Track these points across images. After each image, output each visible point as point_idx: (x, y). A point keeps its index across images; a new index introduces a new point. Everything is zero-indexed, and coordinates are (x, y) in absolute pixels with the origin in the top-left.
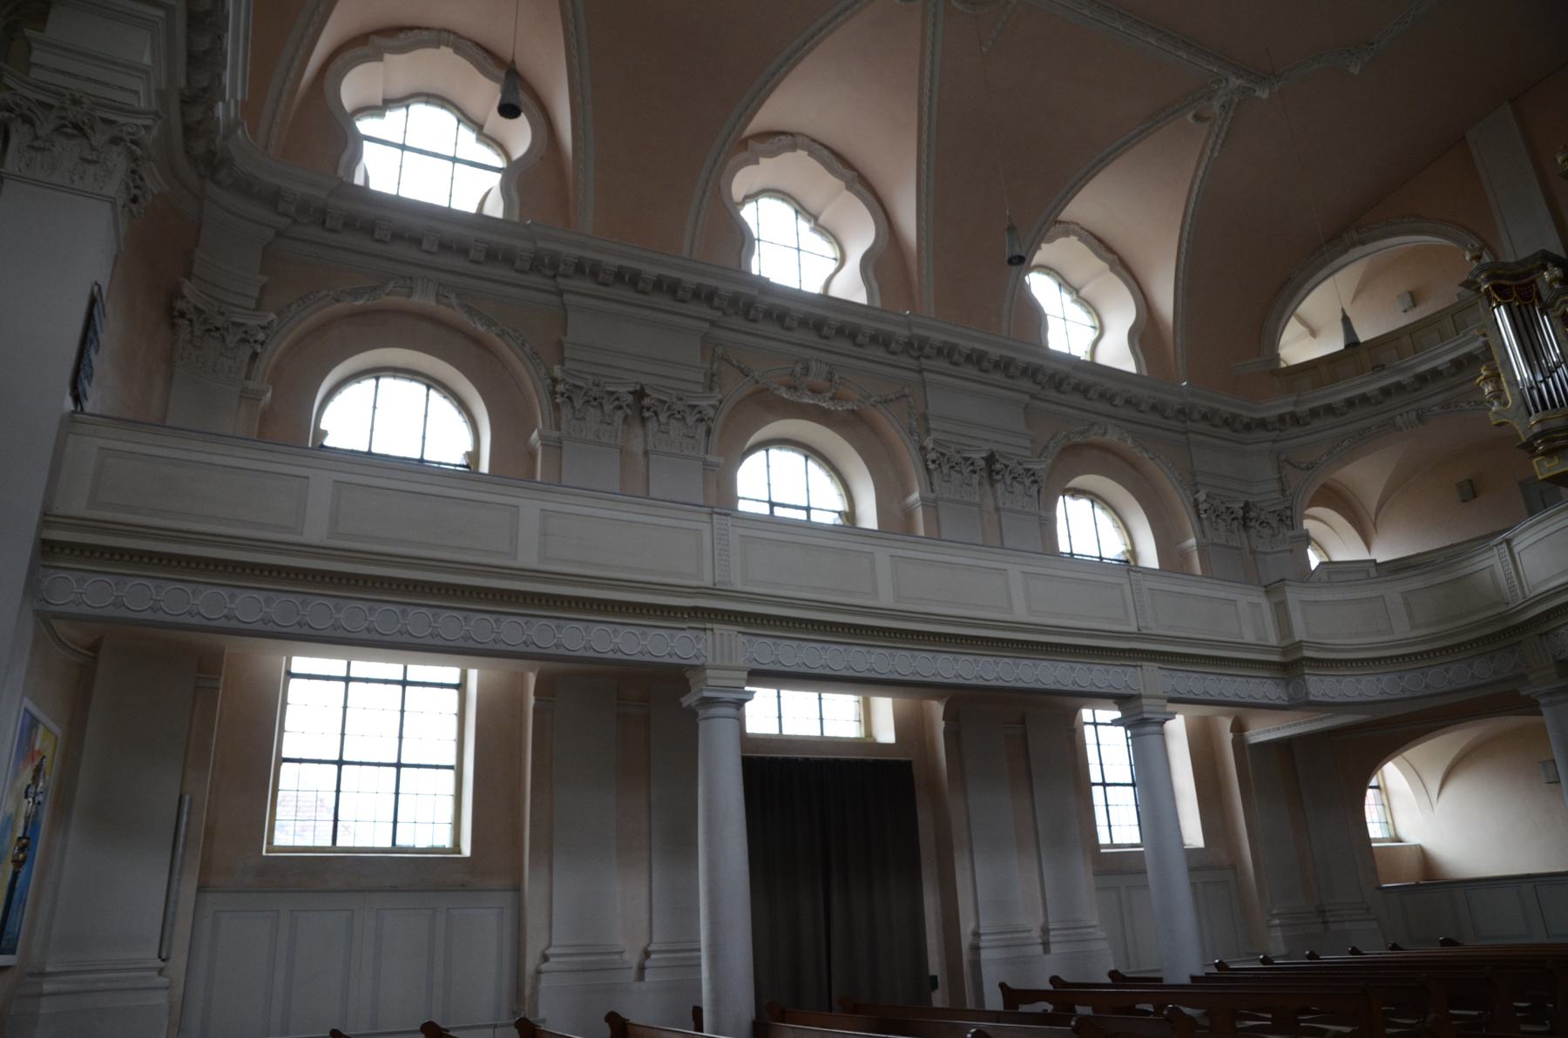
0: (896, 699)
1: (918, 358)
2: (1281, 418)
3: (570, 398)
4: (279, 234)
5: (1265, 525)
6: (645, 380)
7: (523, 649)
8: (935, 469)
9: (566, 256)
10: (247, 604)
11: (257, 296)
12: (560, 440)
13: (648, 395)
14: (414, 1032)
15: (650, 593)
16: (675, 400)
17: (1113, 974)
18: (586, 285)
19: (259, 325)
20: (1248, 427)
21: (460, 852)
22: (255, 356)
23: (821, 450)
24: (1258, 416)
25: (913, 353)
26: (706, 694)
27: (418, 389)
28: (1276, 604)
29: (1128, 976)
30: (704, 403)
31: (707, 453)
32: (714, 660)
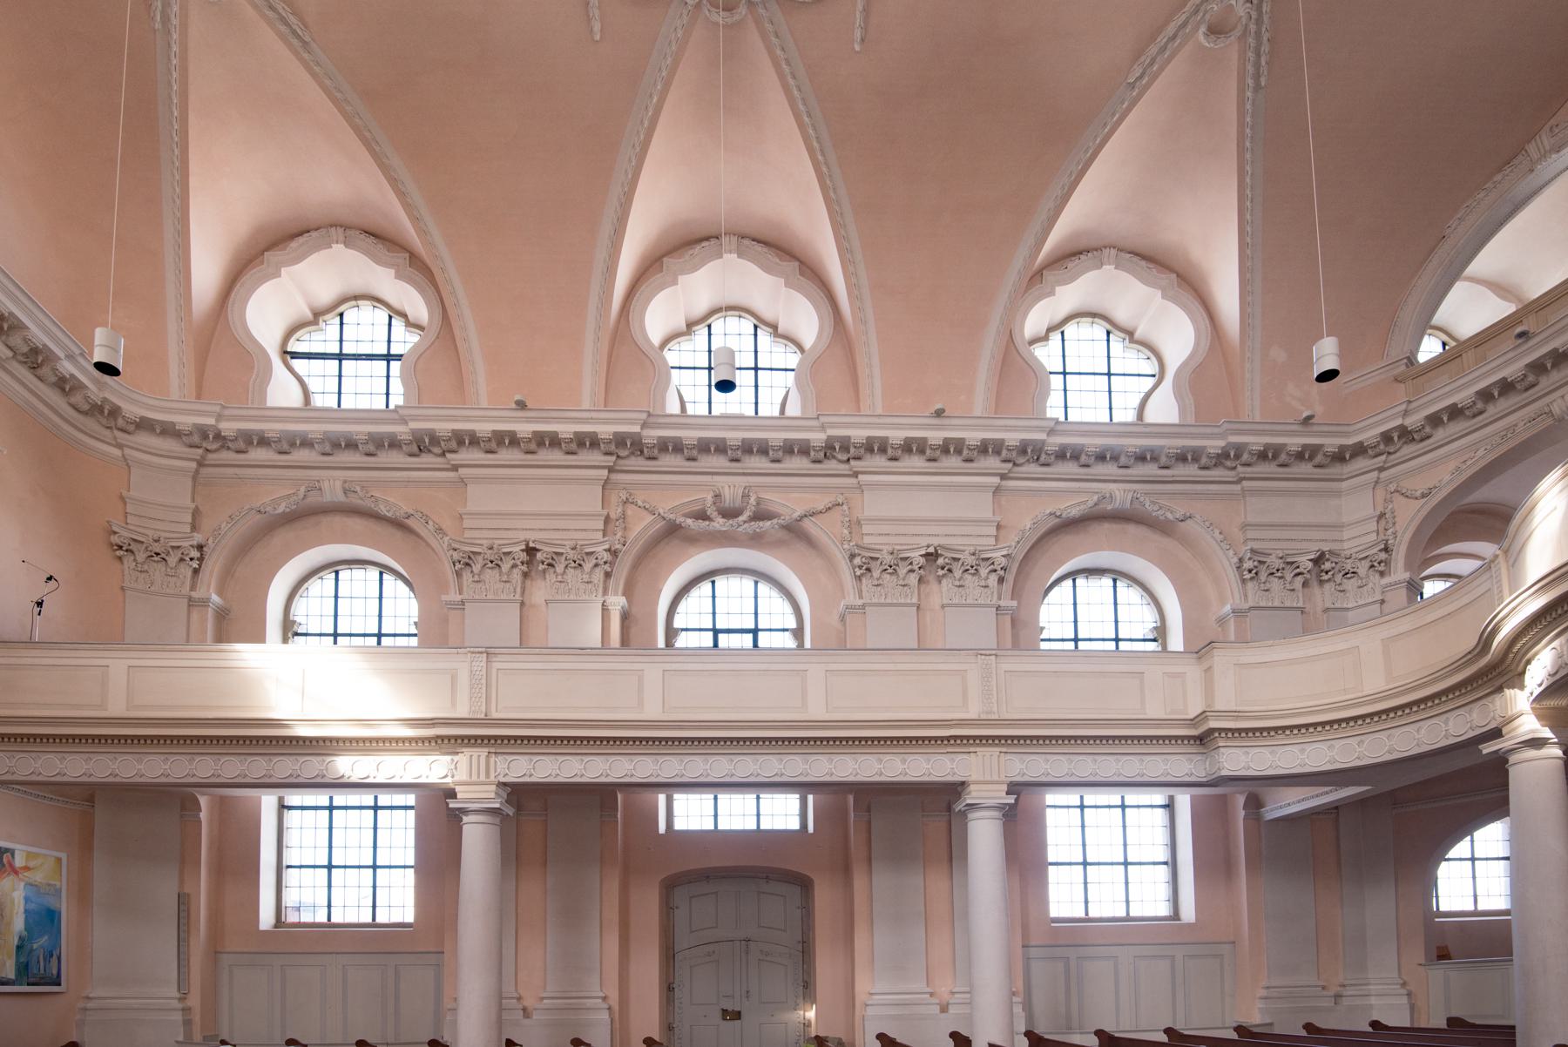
0: (818, 796)
1: (443, 454)
2: (1387, 438)
3: (868, 570)
4: (201, 464)
5: (1348, 576)
6: (531, 536)
7: (1187, 779)
8: (1252, 579)
9: (1169, 449)
10: (231, 767)
11: (190, 520)
12: (463, 603)
13: (941, 555)
14: (352, 1044)
15: (153, 727)
16: (569, 551)
17: (1169, 1031)
18: (879, 461)
19: (191, 546)
20: (1340, 457)
21: (1179, 920)
22: (1001, 580)
23: (1132, 574)
24: (1351, 441)
25: (1228, 463)
26: (969, 801)
27: (747, 583)
28: (1206, 671)
29: (1186, 1033)
30: (185, 544)
31: (191, 590)
32: (479, 777)
